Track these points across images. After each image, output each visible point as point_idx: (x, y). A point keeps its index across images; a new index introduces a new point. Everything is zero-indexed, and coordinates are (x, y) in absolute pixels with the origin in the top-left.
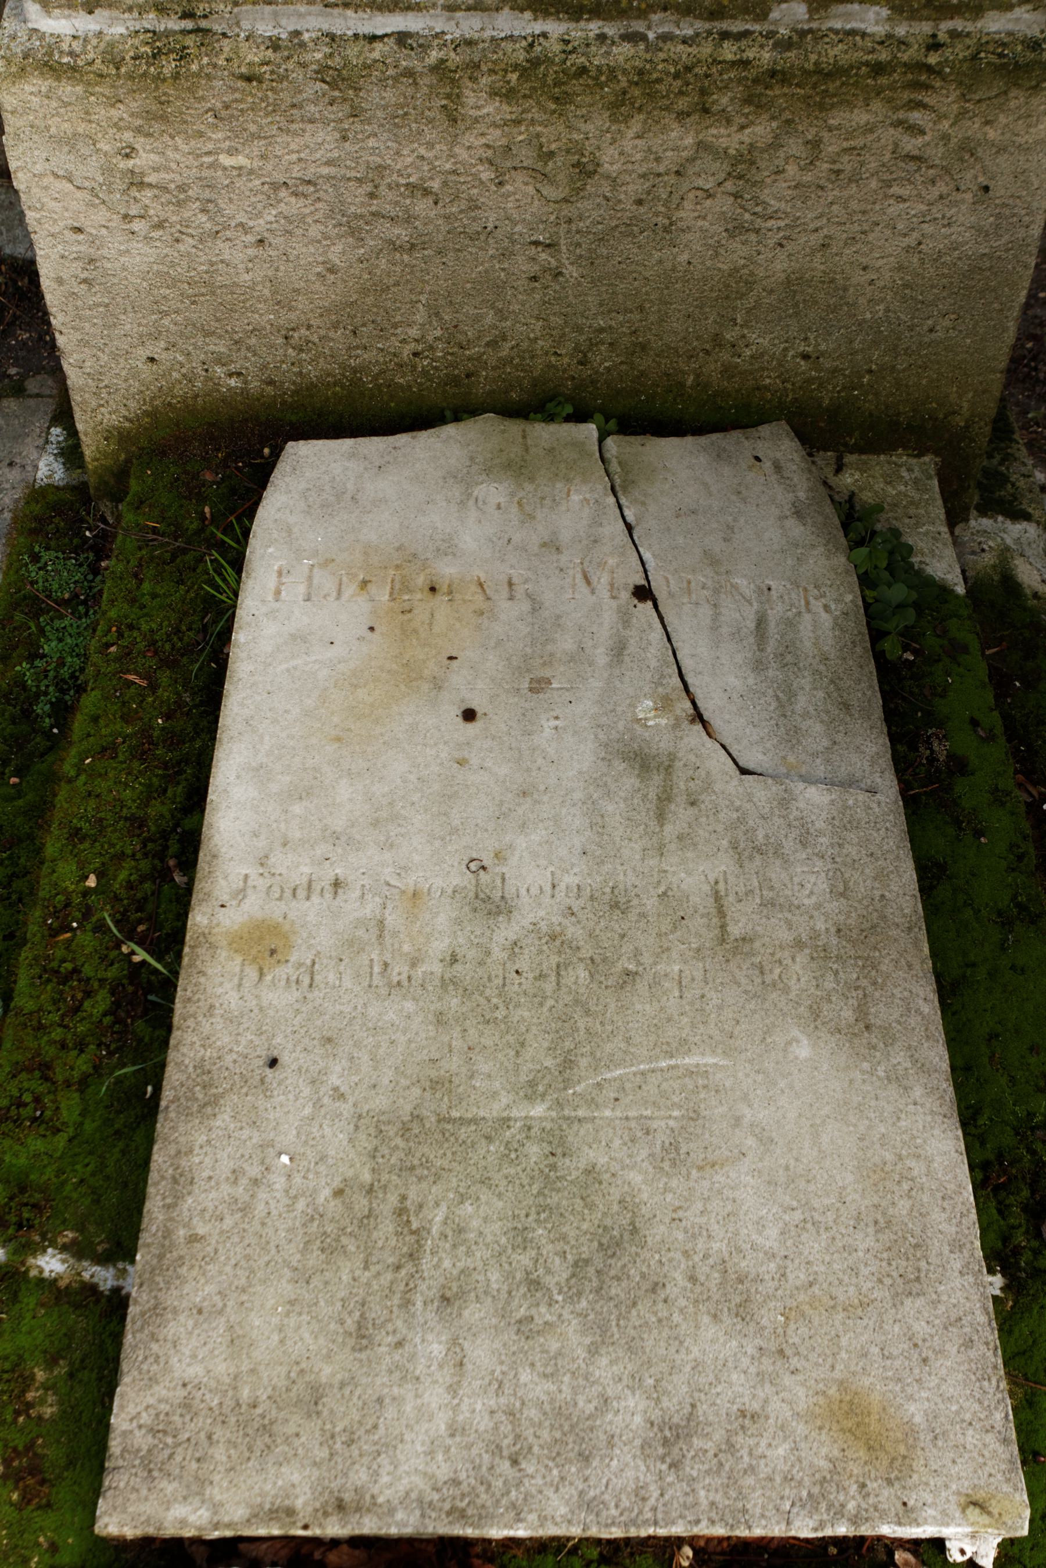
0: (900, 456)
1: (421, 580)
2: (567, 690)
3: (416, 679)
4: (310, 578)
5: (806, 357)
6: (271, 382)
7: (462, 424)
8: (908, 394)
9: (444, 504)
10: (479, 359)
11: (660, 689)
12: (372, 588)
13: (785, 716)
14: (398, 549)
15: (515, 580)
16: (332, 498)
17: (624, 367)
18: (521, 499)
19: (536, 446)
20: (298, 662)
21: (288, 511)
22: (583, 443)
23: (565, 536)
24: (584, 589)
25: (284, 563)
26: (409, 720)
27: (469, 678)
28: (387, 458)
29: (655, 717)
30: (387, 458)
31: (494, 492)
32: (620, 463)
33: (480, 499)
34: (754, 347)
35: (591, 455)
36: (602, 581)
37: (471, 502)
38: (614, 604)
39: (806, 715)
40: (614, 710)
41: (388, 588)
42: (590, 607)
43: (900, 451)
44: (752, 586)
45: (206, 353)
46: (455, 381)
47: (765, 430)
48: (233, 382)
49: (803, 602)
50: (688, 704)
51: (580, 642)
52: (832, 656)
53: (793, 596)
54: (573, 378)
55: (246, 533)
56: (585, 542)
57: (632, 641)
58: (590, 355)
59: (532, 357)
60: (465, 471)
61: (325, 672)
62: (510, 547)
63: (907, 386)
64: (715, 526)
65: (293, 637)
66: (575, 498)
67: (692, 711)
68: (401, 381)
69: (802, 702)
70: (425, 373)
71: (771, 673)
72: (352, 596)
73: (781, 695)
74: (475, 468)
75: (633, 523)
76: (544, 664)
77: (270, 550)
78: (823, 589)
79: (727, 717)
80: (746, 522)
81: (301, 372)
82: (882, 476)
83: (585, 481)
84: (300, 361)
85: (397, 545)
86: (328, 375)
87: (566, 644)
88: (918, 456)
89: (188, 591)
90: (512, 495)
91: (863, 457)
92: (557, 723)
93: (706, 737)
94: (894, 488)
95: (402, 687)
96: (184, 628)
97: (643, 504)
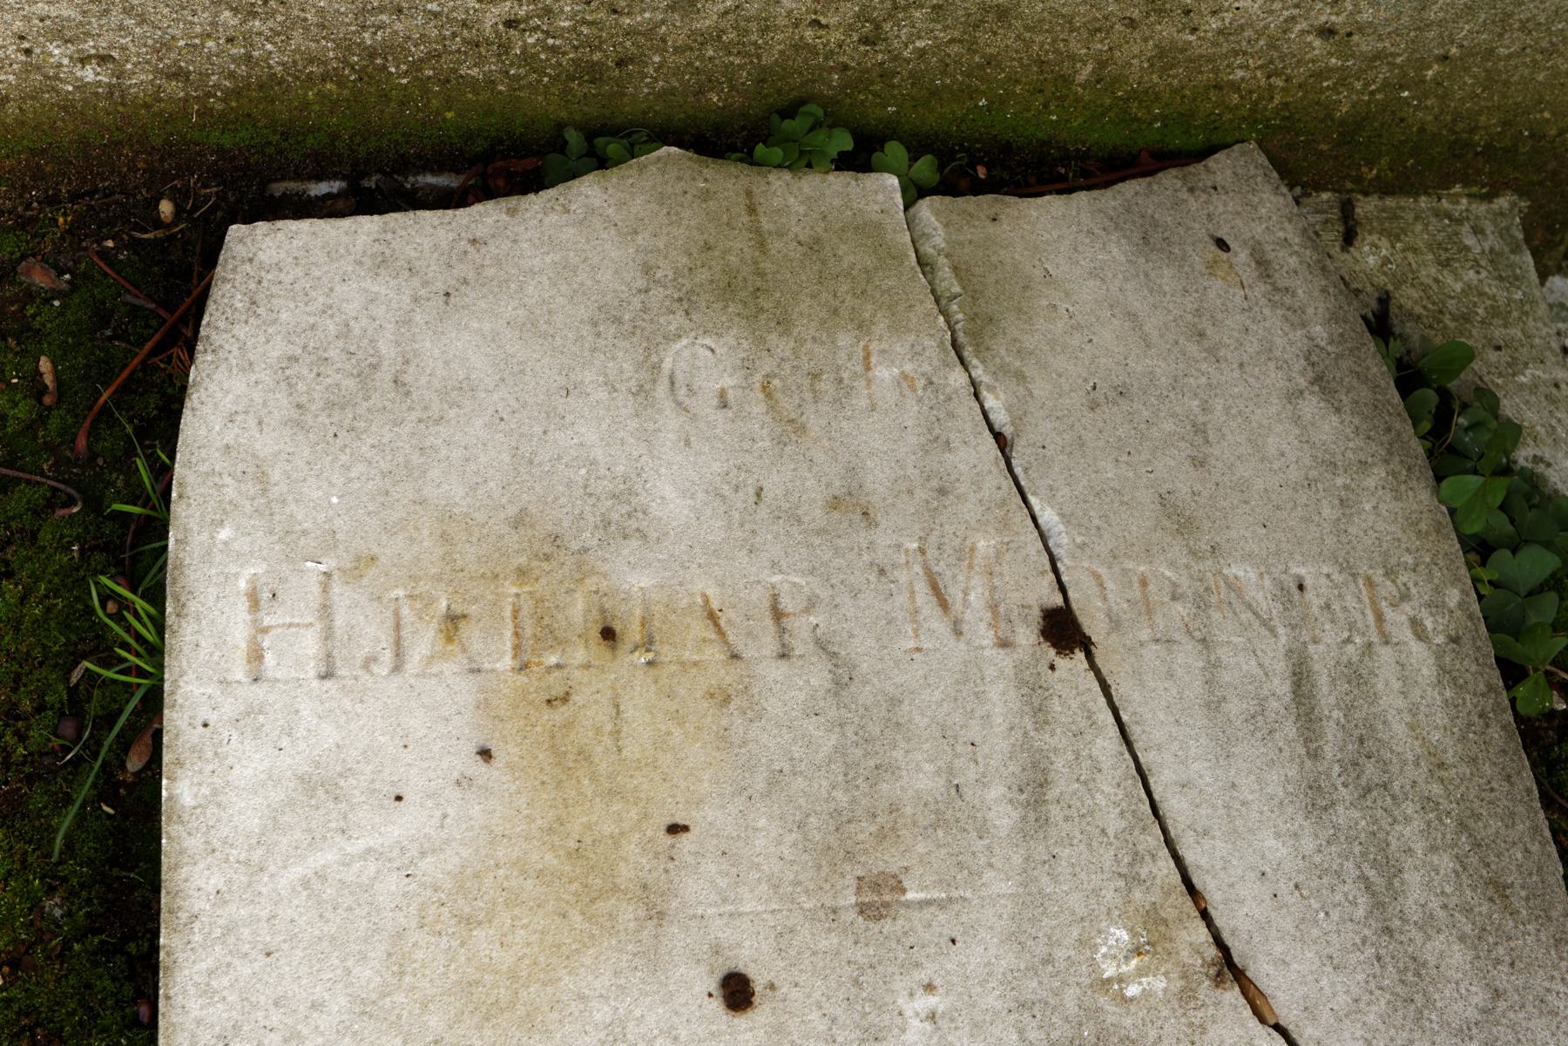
0: (1455, 199)
1: (578, 611)
2: (942, 905)
3: (601, 895)
4: (326, 611)
5: (1327, 32)
6: (178, 74)
7: (614, 175)
8: (1504, 96)
9: (603, 395)
10: (649, 33)
11: (1137, 895)
12: (472, 634)
13: (1388, 931)
14: (518, 522)
15: (787, 603)
16: (350, 384)
17: (955, 49)
18: (768, 377)
19: (781, 234)
20: (325, 857)
21: (252, 422)
22: (878, 226)
23: (877, 479)
24: (938, 624)
25: (260, 569)
26: (602, 1013)
27: (722, 882)
28: (461, 270)
29: (1141, 972)
30: (461, 270)
31: (707, 359)
32: (955, 269)
33: (680, 378)
34: (1228, 16)
35: (900, 258)
36: (973, 597)
37: (662, 388)
38: (1005, 660)
39: (1427, 924)
40: (1048, 960)
41: (508, 633)
42: (961, 677)
43: (1457, 189)
44: (1267, 582)
45: (27, 19)
46: (594, 73)
47: (1221, 166)
48: (89, 74)
49: (1371, 618)
50: (1202, 934)
51: (950, 770)
52: (1449, 757)
53: (1350, 602)
54: (845, 67)
55: (163, 473)
56: (921, 494)
57: (1059, 763)
58: (887, 27)
59: (764, 30)
60: (636, 302)
61: (392, 884)
62: (763, 512)
63: (1506, 83)
64: (1168, 426)
65: (307, 784)
66: (884, 373)
67: (1212, 952)
68: (474, 72)
69: (1415, 891)
70: (527, 57)
71: (1342, 815)
72: (430, 660)
73: (1371, 873)
74: (658, 293)
75: (1008, 431)
76: (881, 836)
77: (224, 534)
78: (1403, 578)
79: (1278, 948)
80: (1227, 409)
81: (248, 57)
82: (1430, 247)
83: (898, 328)
84: (248, 39)
85: (512, 510)
86: (311, 61)
87: (920, 779)
88: (1488, 198)
89: (23, 600)
90: (748, 366)
91: (1390, 202)
92: (932, 1001)
93: (1253, 1022)
94: (1457, 277)
95: (576, 917)
96: (26, 705)
97: (1020, 377)
